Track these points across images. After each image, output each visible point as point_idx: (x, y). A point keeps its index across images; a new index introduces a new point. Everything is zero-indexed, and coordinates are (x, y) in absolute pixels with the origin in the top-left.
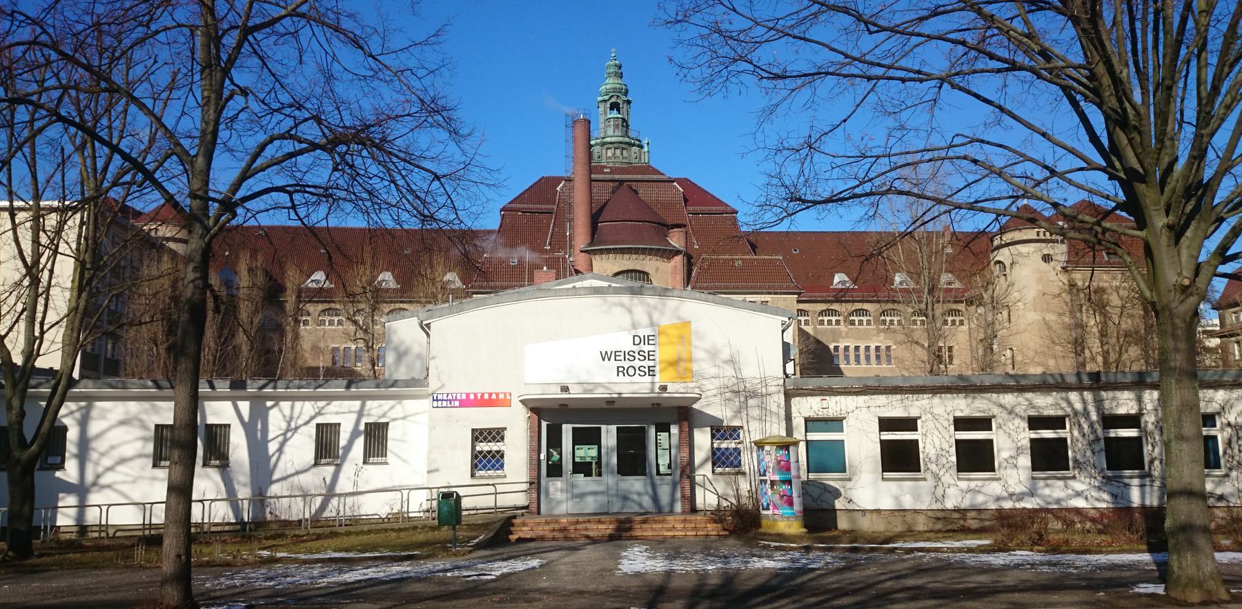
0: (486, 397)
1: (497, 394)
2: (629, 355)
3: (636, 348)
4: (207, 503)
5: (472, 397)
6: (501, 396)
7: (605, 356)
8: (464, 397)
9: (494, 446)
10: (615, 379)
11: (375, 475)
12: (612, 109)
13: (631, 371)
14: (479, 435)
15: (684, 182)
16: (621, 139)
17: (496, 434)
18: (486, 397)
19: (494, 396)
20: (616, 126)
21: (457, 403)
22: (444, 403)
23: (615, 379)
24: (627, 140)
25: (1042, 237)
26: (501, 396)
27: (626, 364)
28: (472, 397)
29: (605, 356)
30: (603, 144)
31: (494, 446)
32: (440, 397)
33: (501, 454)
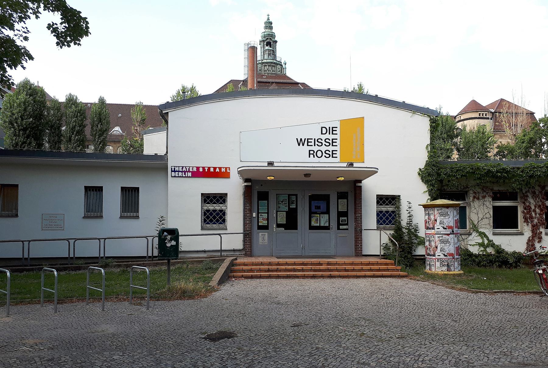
0: (212, 170)
1: (220, 168)
2: (318, 142)
3: (324, 137)
4: (72, 242)
5: (201, 170)
6: (223, 170)
7: (300, 142)
8: (195, 169)
9: (217, 207)
10: (308, 159)
11: (130, 227)
12: (267, 45)
13: (319, 154)
14: (207, 198)
15: (303, 84)
16: (272, 61)
17: (221, 198)
18: (212, 170)
19: (218, 170)
20: (269, 54)
21: (190, 174)
22: (180, 174)
23: (308, 159)
24: (275, 61)
25: (481, 116)
26: (223, 170)
27: (316, 148)
28: (201, 170)
29: (300, 142)
30: (263, 63)
31: (217, 207)
32: (177, 169)
33: (223, 213)
